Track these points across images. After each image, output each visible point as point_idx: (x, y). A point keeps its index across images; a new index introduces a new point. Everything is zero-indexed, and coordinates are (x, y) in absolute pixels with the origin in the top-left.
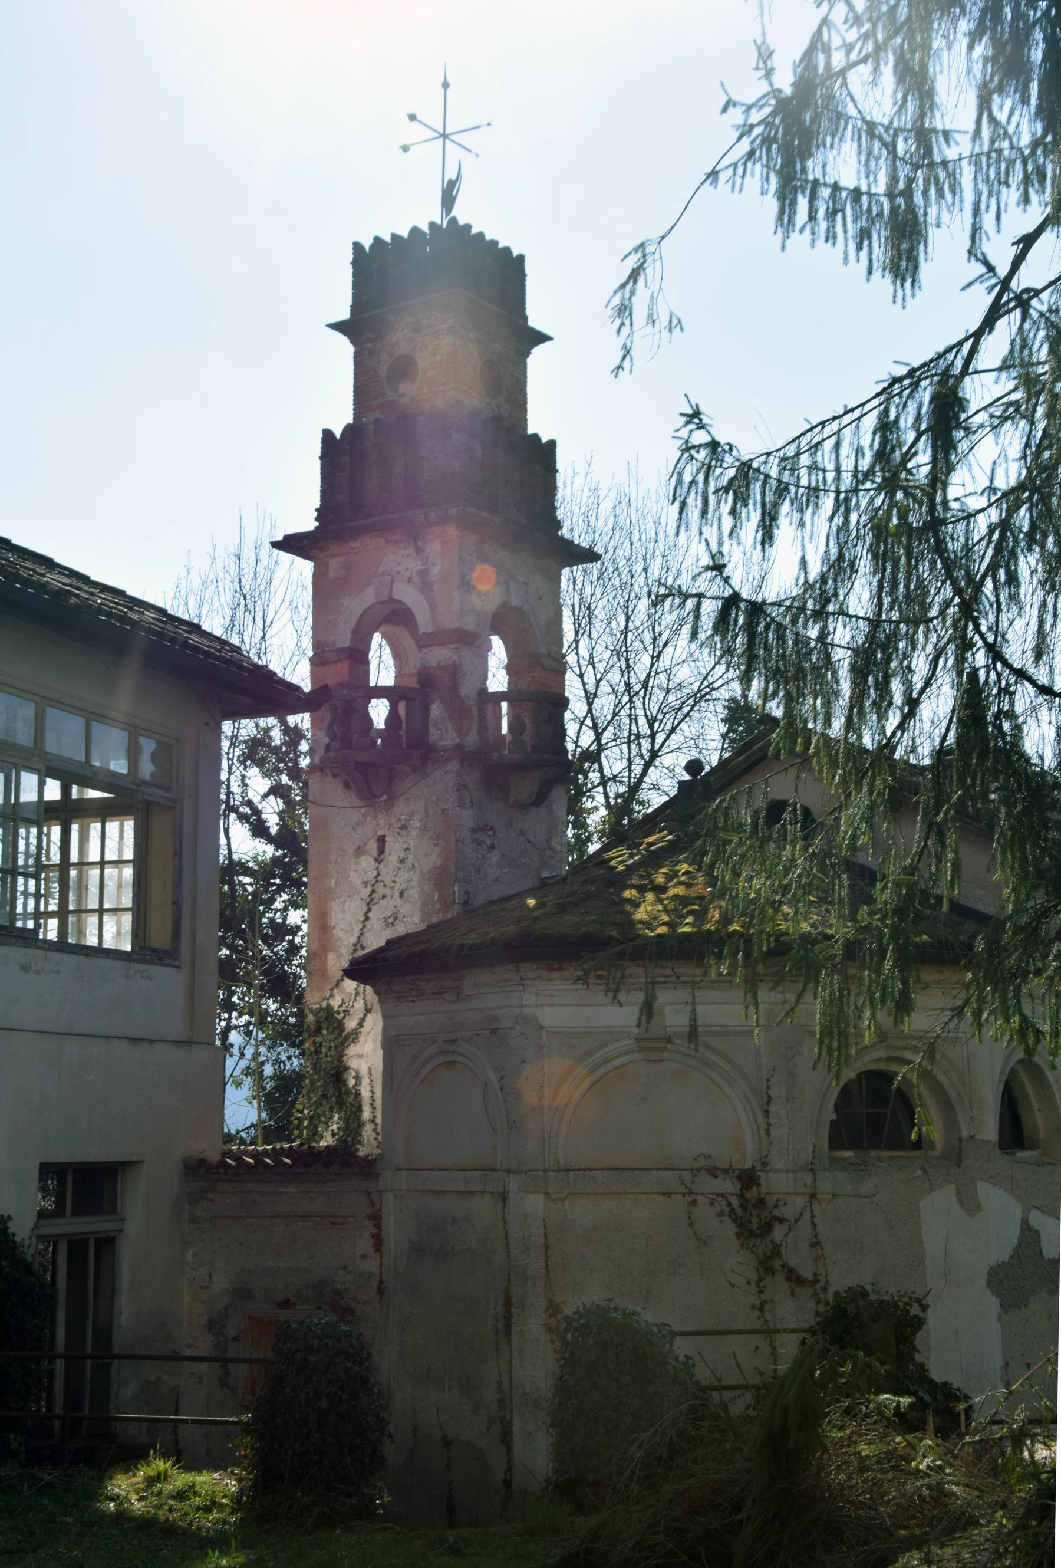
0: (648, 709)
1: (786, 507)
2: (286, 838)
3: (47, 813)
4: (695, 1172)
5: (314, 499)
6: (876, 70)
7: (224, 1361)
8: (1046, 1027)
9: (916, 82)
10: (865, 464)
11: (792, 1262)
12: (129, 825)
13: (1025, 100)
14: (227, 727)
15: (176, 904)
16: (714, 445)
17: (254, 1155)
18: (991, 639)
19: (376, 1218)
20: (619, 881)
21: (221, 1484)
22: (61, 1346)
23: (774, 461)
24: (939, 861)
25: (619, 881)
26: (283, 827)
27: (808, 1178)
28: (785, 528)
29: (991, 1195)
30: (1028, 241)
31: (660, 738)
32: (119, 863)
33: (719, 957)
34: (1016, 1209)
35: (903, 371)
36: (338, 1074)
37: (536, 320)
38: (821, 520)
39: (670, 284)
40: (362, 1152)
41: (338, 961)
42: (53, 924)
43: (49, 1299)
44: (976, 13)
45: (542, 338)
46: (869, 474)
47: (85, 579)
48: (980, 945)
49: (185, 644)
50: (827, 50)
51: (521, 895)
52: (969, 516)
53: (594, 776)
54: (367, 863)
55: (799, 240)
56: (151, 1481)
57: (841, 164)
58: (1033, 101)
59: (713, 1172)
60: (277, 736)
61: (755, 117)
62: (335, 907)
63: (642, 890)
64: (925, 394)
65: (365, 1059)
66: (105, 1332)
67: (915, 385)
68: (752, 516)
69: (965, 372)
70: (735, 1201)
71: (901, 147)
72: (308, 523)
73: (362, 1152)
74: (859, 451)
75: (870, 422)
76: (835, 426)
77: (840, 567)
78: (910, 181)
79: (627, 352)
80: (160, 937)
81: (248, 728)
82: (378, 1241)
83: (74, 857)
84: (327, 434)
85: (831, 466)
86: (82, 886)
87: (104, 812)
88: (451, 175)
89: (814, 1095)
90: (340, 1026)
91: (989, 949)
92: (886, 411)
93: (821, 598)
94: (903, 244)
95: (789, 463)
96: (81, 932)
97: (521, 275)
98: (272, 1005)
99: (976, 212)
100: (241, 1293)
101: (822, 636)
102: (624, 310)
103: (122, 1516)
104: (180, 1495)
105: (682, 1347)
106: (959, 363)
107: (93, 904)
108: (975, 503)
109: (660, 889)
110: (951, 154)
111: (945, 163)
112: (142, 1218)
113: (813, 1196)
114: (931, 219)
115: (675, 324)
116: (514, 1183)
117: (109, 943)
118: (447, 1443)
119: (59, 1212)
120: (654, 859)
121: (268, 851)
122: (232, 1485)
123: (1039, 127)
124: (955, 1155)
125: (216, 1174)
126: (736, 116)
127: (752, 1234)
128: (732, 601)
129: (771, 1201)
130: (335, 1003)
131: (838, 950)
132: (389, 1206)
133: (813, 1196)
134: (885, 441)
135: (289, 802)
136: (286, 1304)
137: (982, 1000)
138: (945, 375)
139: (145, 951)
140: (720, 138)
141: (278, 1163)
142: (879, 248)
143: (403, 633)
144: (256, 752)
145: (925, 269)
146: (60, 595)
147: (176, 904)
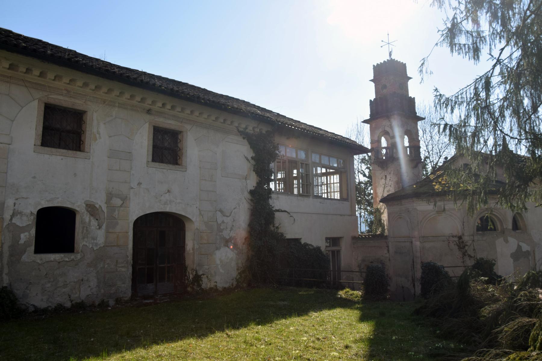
0: (437, 148)
1: (457, 106)
2: (370, 177)
3: (323, 175)
4: (449, 237)
5: (369, 113)
6: (468, 21)
7: (361, 272)
8: (516, 205)
9: (476, 22)
10: (472, 96)
11: (469, 253)
12: (338, 176)
13: (498, 23)
14: (356, 157)
15: (347, 190)
16: (440, 95)
17: (365, 236)
18: (501, 128)
19: (388, 247)
20: (432, 181)
21: (360, 293)
22: (331, 269)
23: (454, 97)
24: (493, 173)
25: (432, 181)
26: (369, 175)
27: (472, 237)
28: (456, 111)
29: (510, 239)
30: (502, 49)
31: (441, 153)
32: (337, 183)
33: (449, 195)
34: (516, 242)
35: (478, 77)
36: (380, 220)
37: (409, 75)
38: (464, 107)
39: (430, 65)
40: (385, 234)
41: (378, 199)
42: (326, 194)
43: (329, 261)
44: (487, 8)
45: (411, 78)
46: (473, 98)
47: (327, 132)
48: (501, 190)
49: (346, 142)
50: (457, 19)
51: (413, 185)
52: (494, 104)
53: (428, 161)
54: (383, 181)
55: (455, 54)
56: (346, 292)
57: (462, 39)
58: (500, 23)
59: (453, 237)
60: (367, 158)
61: (444, 32)
62: (378, 189)
63: (436, 183)
64: (483, 81)
65: (385, 217)
66: (339, 267)
67: (481, 80)
68: (449, 108)
69: (491, 76)
70: (458, 242)
71: (474, 35)
72: (368, 117)
73: (385, 234)
74: (471, 94)
75: (473, 88)
76: (465, 89)
77: (468, 116)
78: (476, 41)
79: (422, 79)
80: (345, 196)
81: (361, 156)
82: (388, 251)
83: (329, 182)
84: (371, 101)
85: (465, 97)
86: (331, 188)
87: (333, 174)
88: (390, 50)
89: (475, 221)
90: (380, 211)
91: (503, 190)
92: (476, 85)
93: (464, 123)
94: (476, 52)
95: (457, 97)
96: (331, 196)
97: (406, 67)
98: (369, 208)
99: (490, 45)
100: (363, 261)
101: (465, 131)
102: (421, 71)
103: (341, 298)
104: (351, 295)
105: (446, 269)
106: (490, 75)
107: (333, 191)
108: (495, 102)
109: (440, 182)
110: (484, 35)
111: (483, 37)
112: (345, 248)
113: (473, 241)
114: (481, 48)
115: (431, 73)
116: (414, 240)
117: (336, 198)
118: (403, 287)
119: (330, 246)
120: (439, 177)
121: (367, 179)
122: (360, 293)
123: (502, 28)
124: (503, 232)
125: (358, 239)
126: (440, 33)
127: (461, 248)
128: (446, 125)
129: (465, 242)
130: (379, 207)
131: (471, 192)
132: (390, 245)
133: (473, 241)
134: (476, 91)
135: (370, 170)
136: (372, 262)
137: (502, 200)
138: (487, 77)
139: (342, 199)
140: (438, 37)
141: (369, 237)
142: (471, 54)
143: (388, 137)
144: (363, 161)
145: (481, 57)
146: (322, 135)
147: (347, 190)
